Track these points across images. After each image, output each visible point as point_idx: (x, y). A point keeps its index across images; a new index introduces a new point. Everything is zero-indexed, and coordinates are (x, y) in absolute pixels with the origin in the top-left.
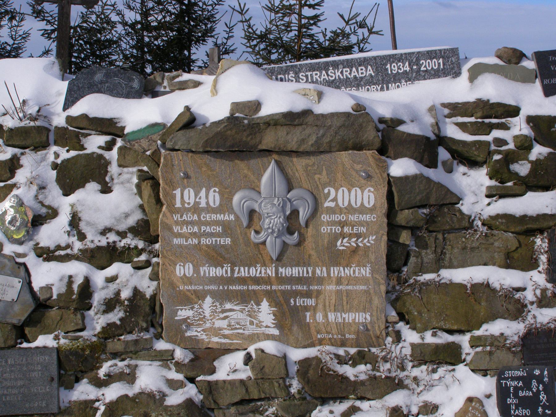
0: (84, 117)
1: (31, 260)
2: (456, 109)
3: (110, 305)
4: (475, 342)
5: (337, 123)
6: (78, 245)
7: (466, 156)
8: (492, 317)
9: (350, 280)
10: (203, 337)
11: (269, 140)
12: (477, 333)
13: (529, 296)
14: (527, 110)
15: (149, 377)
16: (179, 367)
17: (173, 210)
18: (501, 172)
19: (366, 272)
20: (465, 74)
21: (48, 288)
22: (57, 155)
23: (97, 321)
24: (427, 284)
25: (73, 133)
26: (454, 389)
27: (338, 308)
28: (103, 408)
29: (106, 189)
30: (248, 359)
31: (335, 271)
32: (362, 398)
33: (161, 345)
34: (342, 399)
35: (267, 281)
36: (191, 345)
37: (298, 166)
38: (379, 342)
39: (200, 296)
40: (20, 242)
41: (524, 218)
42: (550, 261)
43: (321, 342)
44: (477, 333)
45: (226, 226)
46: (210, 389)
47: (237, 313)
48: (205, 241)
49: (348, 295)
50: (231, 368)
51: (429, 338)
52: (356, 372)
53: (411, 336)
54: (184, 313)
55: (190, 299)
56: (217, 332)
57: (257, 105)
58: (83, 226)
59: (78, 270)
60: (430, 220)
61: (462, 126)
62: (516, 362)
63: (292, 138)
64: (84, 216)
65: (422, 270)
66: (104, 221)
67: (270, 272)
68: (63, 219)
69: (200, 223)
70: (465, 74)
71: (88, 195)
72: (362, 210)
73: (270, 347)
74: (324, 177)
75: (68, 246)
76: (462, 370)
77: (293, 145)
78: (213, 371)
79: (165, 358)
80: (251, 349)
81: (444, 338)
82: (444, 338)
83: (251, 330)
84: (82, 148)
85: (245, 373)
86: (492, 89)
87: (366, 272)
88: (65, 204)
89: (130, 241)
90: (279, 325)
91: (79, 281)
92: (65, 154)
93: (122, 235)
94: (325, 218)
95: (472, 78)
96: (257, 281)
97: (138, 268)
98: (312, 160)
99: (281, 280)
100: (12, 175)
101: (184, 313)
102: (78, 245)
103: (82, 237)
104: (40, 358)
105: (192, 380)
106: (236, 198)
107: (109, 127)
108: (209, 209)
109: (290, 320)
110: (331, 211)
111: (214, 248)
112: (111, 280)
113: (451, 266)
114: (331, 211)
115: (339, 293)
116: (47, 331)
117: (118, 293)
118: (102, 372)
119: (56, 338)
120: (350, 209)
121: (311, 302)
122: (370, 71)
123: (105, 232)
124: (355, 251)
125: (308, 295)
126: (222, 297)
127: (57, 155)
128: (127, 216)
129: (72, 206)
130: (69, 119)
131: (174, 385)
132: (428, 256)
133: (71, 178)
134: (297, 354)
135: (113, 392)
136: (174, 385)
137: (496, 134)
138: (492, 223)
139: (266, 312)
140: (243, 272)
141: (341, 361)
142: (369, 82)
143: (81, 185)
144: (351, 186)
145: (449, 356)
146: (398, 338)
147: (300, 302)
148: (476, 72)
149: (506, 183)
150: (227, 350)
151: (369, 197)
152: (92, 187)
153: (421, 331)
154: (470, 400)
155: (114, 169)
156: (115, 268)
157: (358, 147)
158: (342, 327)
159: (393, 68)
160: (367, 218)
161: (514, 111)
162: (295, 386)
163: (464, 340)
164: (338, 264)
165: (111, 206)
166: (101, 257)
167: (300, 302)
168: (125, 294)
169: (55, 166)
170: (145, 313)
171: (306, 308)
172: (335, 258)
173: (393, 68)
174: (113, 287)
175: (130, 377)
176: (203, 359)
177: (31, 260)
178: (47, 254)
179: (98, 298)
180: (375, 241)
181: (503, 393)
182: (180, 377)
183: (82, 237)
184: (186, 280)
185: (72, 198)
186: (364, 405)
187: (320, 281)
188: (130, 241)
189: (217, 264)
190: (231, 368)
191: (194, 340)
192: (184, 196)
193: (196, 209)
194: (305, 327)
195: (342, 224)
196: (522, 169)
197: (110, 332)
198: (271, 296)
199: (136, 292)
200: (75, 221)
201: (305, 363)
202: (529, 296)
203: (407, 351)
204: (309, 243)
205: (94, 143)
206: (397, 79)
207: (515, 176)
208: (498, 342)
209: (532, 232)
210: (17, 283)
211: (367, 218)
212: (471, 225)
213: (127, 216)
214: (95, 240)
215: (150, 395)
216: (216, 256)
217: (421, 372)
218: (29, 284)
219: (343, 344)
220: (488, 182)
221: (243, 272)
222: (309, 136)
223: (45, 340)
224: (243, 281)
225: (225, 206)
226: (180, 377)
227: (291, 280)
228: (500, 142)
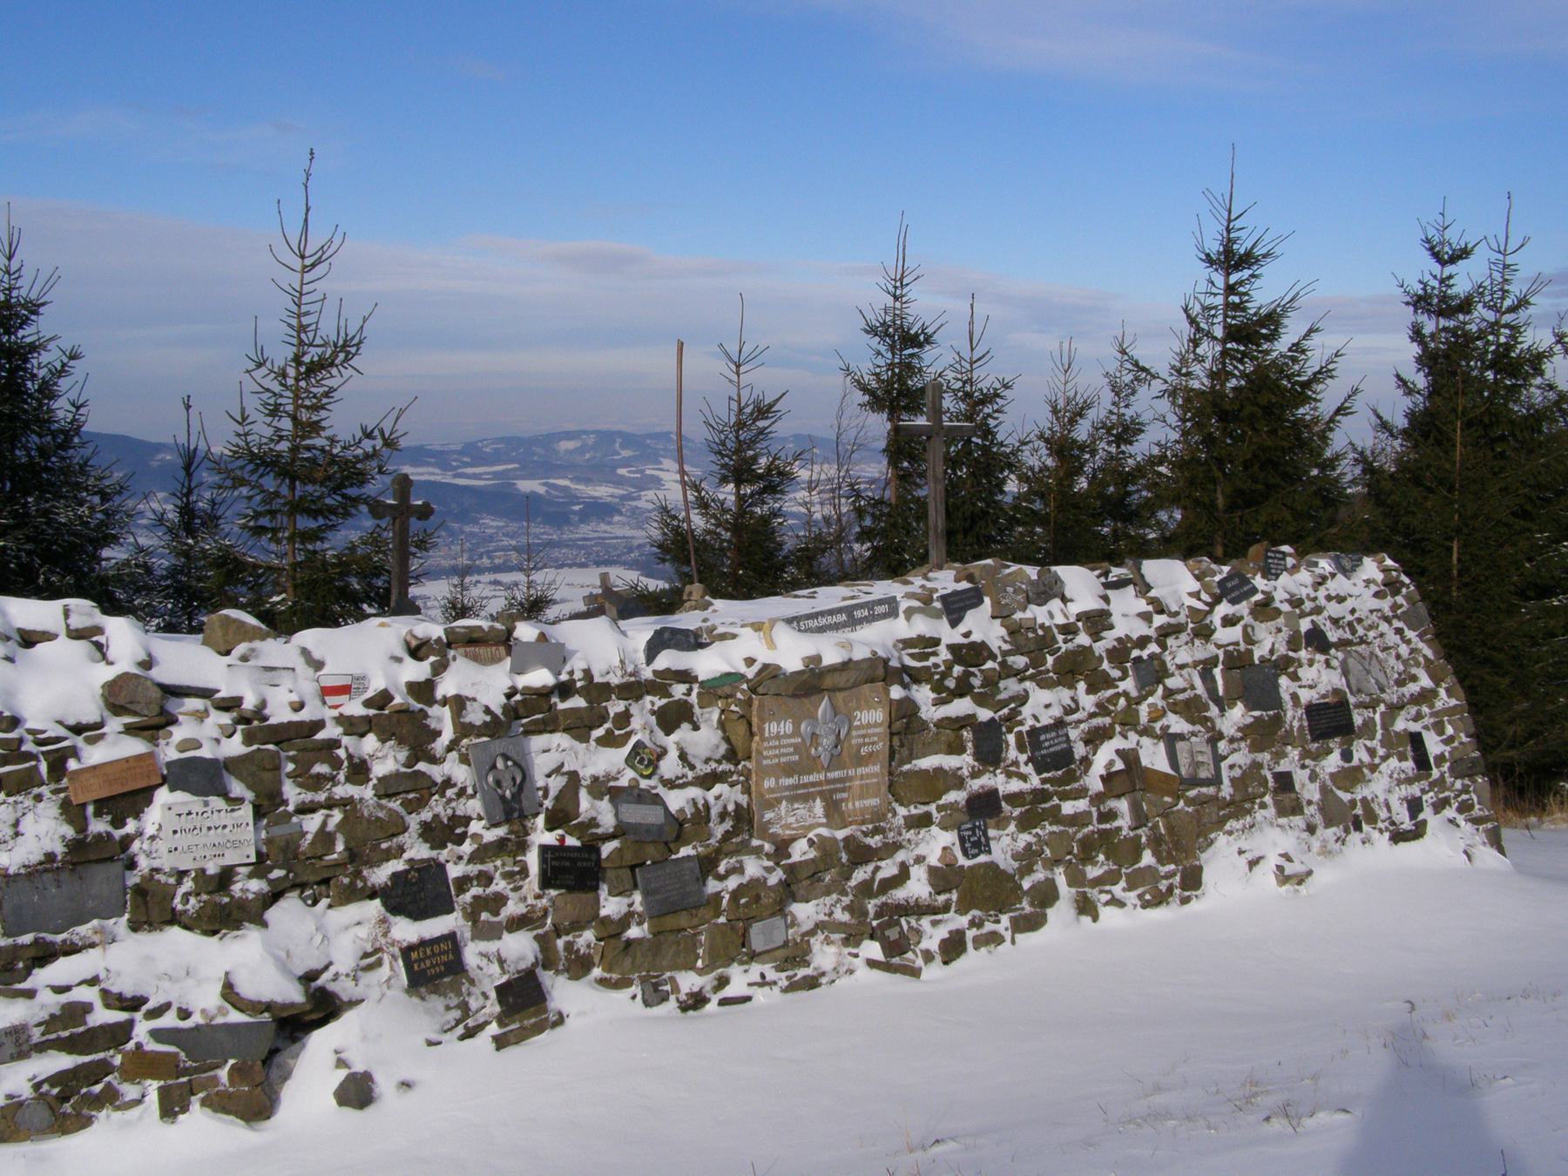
0: (668, 670)
1: (661, 790)
2: (907, 643)
3: (723, 816)
4: (939, 809)
5: (864, 666)
6: (690, 775)
7: (917, 677)
8: (946, 791)
9: (868, 776)
10: (780, 831)
11: (828, 682)
12: (941, 802)
13: (965, 772)
14: (945, 641)
15: (753, 867)
16: (768, 856)
17: (763, 739)
18: (938, 687)
19: (877, 768)
20: (902, 615)
21: (682, 810)
22: (653, 704)
23: (719, 830)
24: (907, 773)
25: (659, 685)
26: (933, 843)
27: (862, 797)
28: (727, 896)
29: (696, 728)
30: (811, 843)
31: (859, 771)
32: (881, 859)
33: (755, 842)
34: (867, 862)
35: (819, 784)
36: (773, 839)
37: (840, 696)
38: (883, 817)
39: (779, 801)
40: (649, 777)
41: (958, 719)
42: (976, 747)
43: (851, 824)
44: (941, 802)
45: (796, 746)
46: (792, 870)
47: (801, 809)
48: (783, 760)
49: (865, 785)
50: (800, 851)
51: (914, 811)
52: (874, 841)
53: (902, 811)
54: (769, 815)
55: (771, 805)
56: (788, 826)
57: (817, 659)
58: (690, 758)
59: (694, 792)
60: (907, 726)
61: (912, 656)
62: (966, 818)
63: (840, 679)
64: (689, 750)
65: (902, 763)
66: (705, 754)
67: (822, 777)
68: (673, 754)
69: (779, 747)
70: (902, 615)
71: (683, 733)
72: (876, 725)
73: (824, 831)
74: (853, 704)
75: (684, 776)
76: (934, 829)
77: (842, 685)
78: (789, 856)
79: (758, 851)
80: (811, 835)
81: (922, 809)
82: (922, 809)
83: (810, 821)
84: (671, 696)
85: (812, 854)
86: (922, 626)
87: (877, 768)
88: (671, 741)
89: (725, 766)
90: (827, 815)
91: (701, 803)
92: (660, 702)
93: (719, 762)
94: (854, 733)
95: (908, 619)
96: (813, 784)
97: (732, 785)
98: (847, 693)
99: (828, 782)
100: (629, 724)
101: (769, 815)
102: (690, 775)
103: (692, 767)
104: (686, 865)
105: (777, 864)
106: (803, 727)
107: (685, 676)
108: (786, 736)
109: (834, 812)
110: (858, 728)
111: (788, 764)
112: (718, 798)
113: (918, 758)
114: (858, 728)
115: (861, 786)
116: (686, 843)
117: (725, 807)
118: (722, 869)
119: (695, 847)
120: (869, 726)
121: (845, 795)
122: (844, 617)
123: (707, 761)
124: (871, 754)
125: (843, 790)
126: (792, 799)
127: (653, 704)
128: (717, 747)
129: (677, 744)
130: (655, 672)
131: (769, 870)
132: (905, 752)
133: (672, 717)
134: (840, 834)
135: (733, 883)
136: (769, 870)
137: (933, 660)
138: (944, 723)
139: (818, 807)
140: (806, 779)
141: (865, 834)
142: (843, 625)
143: (677, 726)
144: (869, 709)
145: (924, 821)
146: (895, 814)
147: (839, 796)
148: (909, 613)
149: (945, 695)
150: (793, 839)
151: (878, 716)
152: (686, 726)
153: (906, 806)
154: (945, 849)
155: (697, 710)
156: (719, 788)
157: (872, 681)
158: (863, 810)
159: (858, 614)
160: (877, 730)
161: (936, 642)
162: (844, 857)
163: (932, 808)
164: (860, 765)
165: (703, 739)
166: (707, 781)
167: (839, 796)
168: (731, 807)
169: (653, 713)
170: (743, 819)
171: (842, 800)
172: (860, 761)
173: (858, 614)
174: (720, 803)
175: (739, 870)
176: (782, 848)
177: (661, 790)
178: (671, 784)
179: (714, 812)
180: (881, 746)
181: (962, 840)
182: (771, 864)
183: (692, 767)
184: (771, 790)
185: (674, 737)
186: (882, 864)
187: (850, 779)
188: (725, 766)
189: (790, 775)
190: (800, 851)
191: (774, 835)
192: (772, 728)
193: (778, 737)
194: (841, 813)
195: (864, 736)
196: (951, 683)
197: (727, 836)
198: (821, 794)
199: (737, 804)
200: (683, 756)
201: (846, 839)
202: (965, 772)
203: (902, 822)
204: (845, 753)
205: (679, 690)
206: (861, 621)
207: (947, 689)
208: (952, 806)
209: (962, 727)
210: (659, 810)
211: (877, 730)
212: (928, 728)
213: (717, 747)
214: (703, 769)
215: (758, 880)
216: (789, 770)
217: (910, 835)
218: (666, 809)
219: (863, 822)
220: (933, 695)
221: (806, 779)
222: (852, 676)
223: (685, 851)
224: (805, 786)
225: (796, 732)
226: (771, 864)
227: (835, 781)
228: (936, 666)
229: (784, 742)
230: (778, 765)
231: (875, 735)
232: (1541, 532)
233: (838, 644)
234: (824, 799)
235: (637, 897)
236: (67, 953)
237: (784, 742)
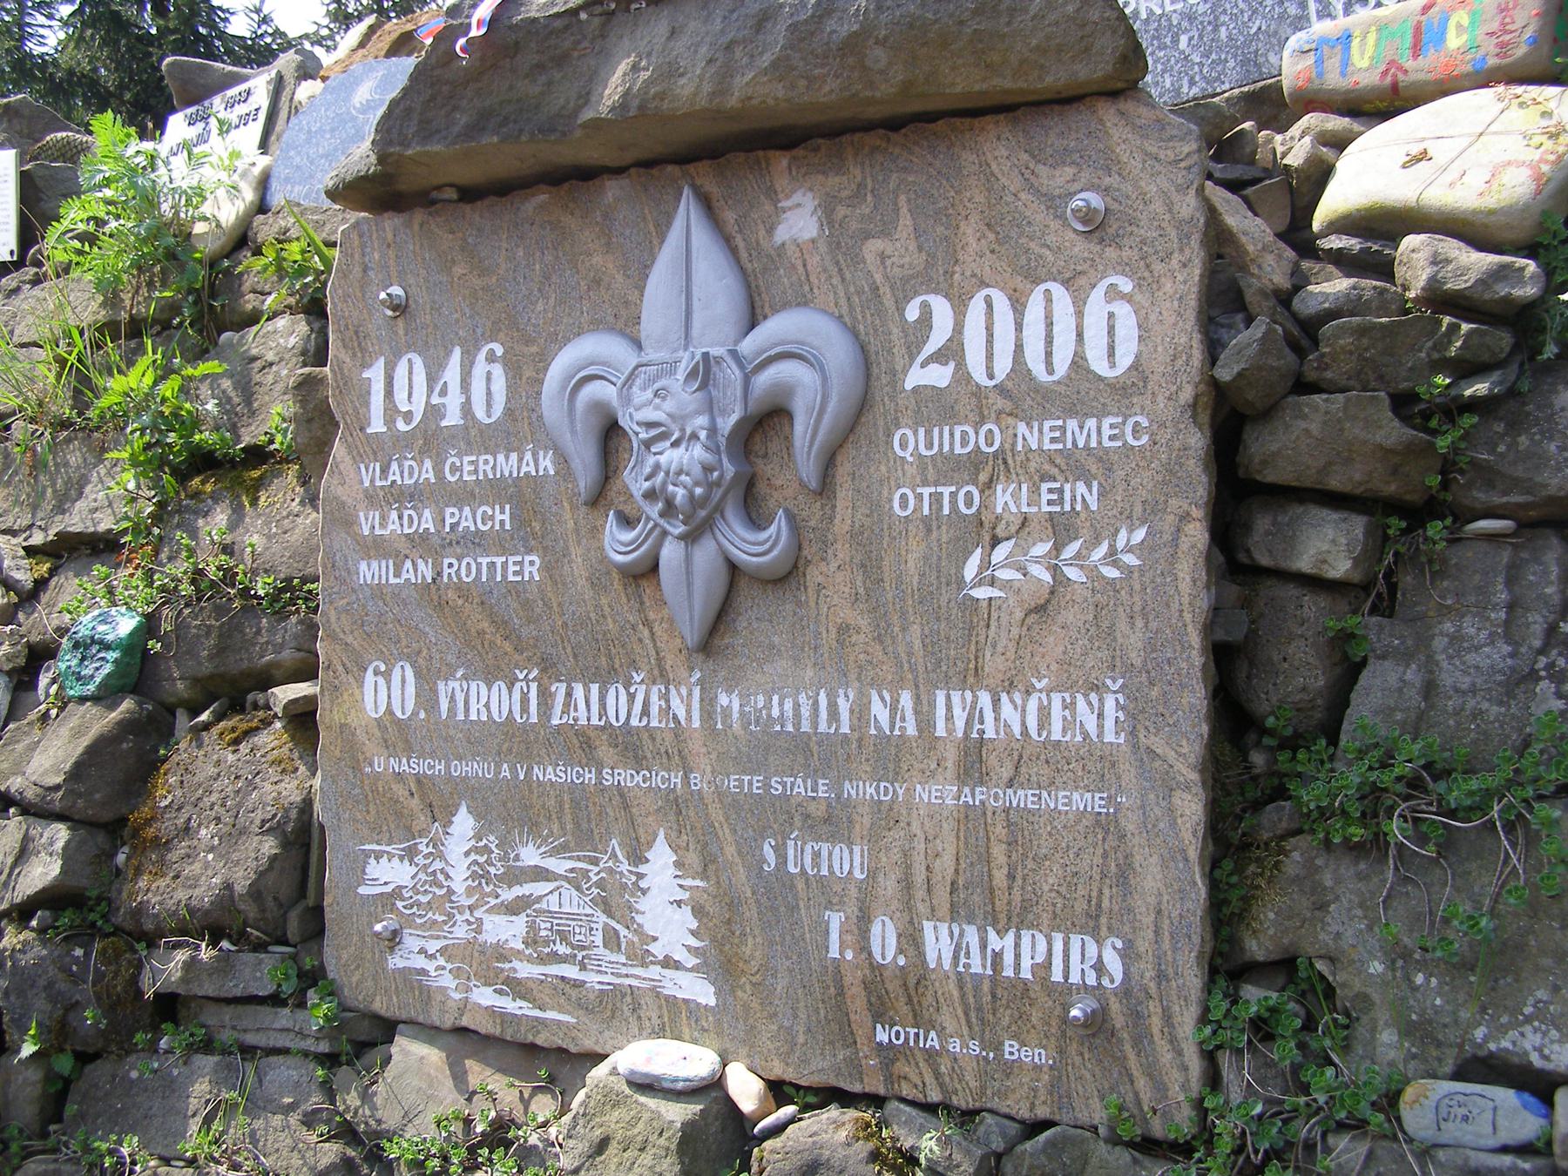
9: (1033, 760)
31: (953, 711)
55: (413, 814)
72: (1081, 392)
94: (909, 443)
96: (631, 745)
101: (389, 872)
108: (476, 437)
114: (935, 408)
120: (1022, 395)
121: (846, 861)
125: (832, 823)
126: (512, 813)
140: (584, 705)
144: (1024, 275)
147: (803, 856)
171: (827, 891)
184: (398, 735)
193: (430, 438)
221: (584, 705)
224: (581, 744)
229: (469, 467)
230: (432, 593)
231: (1072, 465)
232: (126, 45)
233: (90, 133)
234: (701, 857)
235: (391, 966)
236: (1445, 93)
237: (469, 467)
